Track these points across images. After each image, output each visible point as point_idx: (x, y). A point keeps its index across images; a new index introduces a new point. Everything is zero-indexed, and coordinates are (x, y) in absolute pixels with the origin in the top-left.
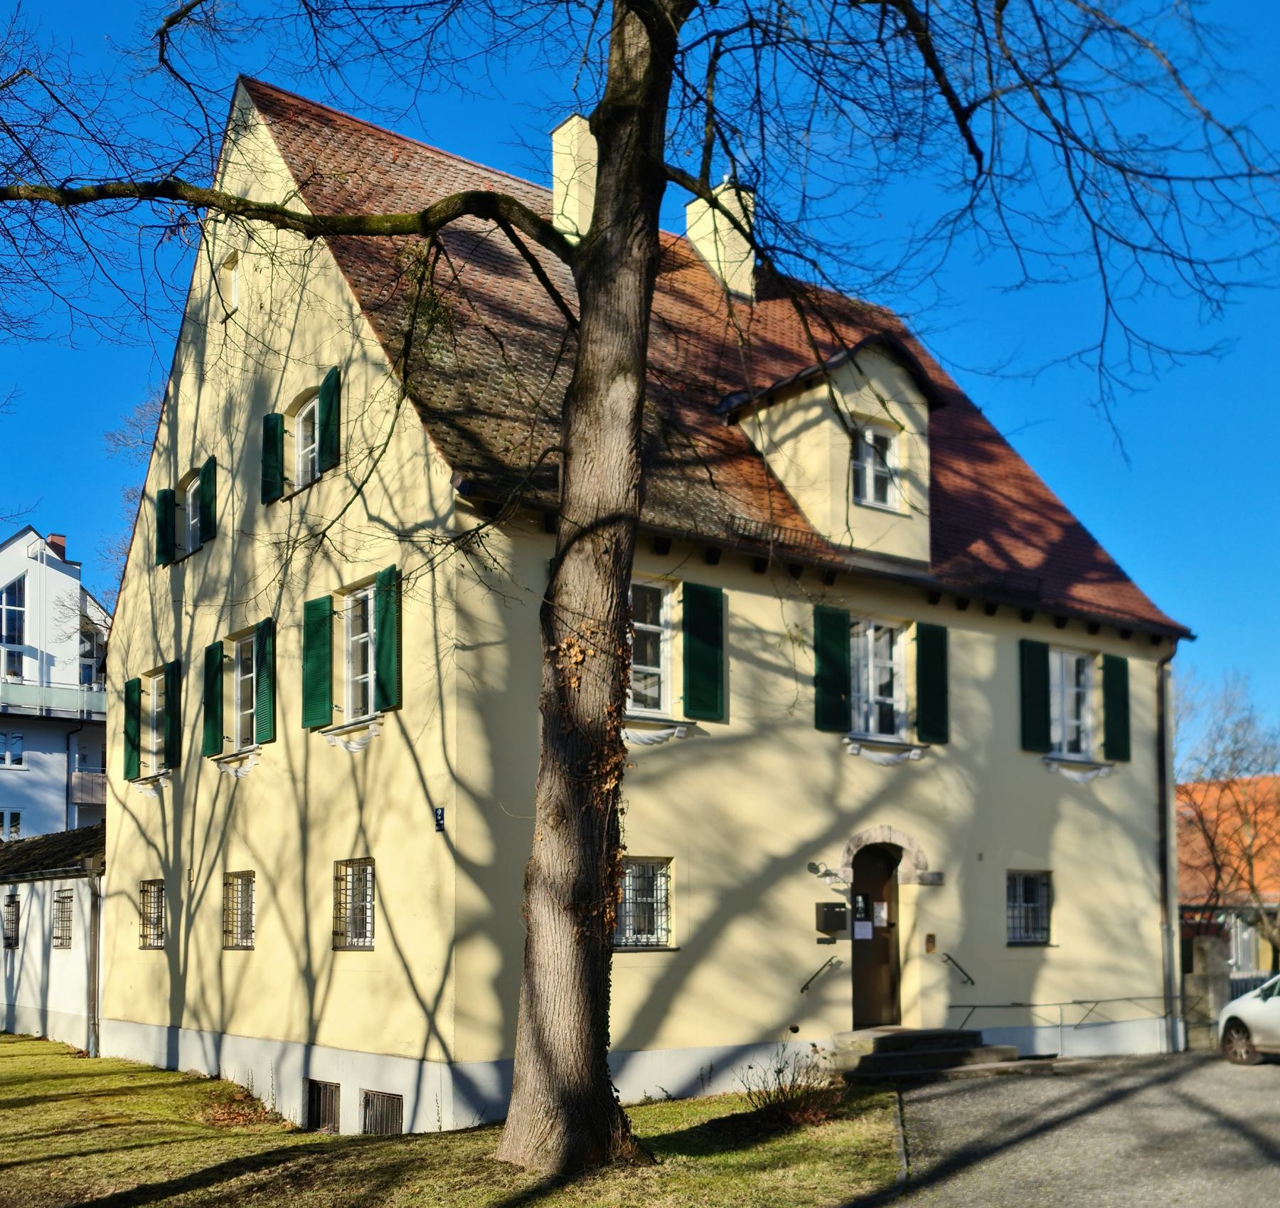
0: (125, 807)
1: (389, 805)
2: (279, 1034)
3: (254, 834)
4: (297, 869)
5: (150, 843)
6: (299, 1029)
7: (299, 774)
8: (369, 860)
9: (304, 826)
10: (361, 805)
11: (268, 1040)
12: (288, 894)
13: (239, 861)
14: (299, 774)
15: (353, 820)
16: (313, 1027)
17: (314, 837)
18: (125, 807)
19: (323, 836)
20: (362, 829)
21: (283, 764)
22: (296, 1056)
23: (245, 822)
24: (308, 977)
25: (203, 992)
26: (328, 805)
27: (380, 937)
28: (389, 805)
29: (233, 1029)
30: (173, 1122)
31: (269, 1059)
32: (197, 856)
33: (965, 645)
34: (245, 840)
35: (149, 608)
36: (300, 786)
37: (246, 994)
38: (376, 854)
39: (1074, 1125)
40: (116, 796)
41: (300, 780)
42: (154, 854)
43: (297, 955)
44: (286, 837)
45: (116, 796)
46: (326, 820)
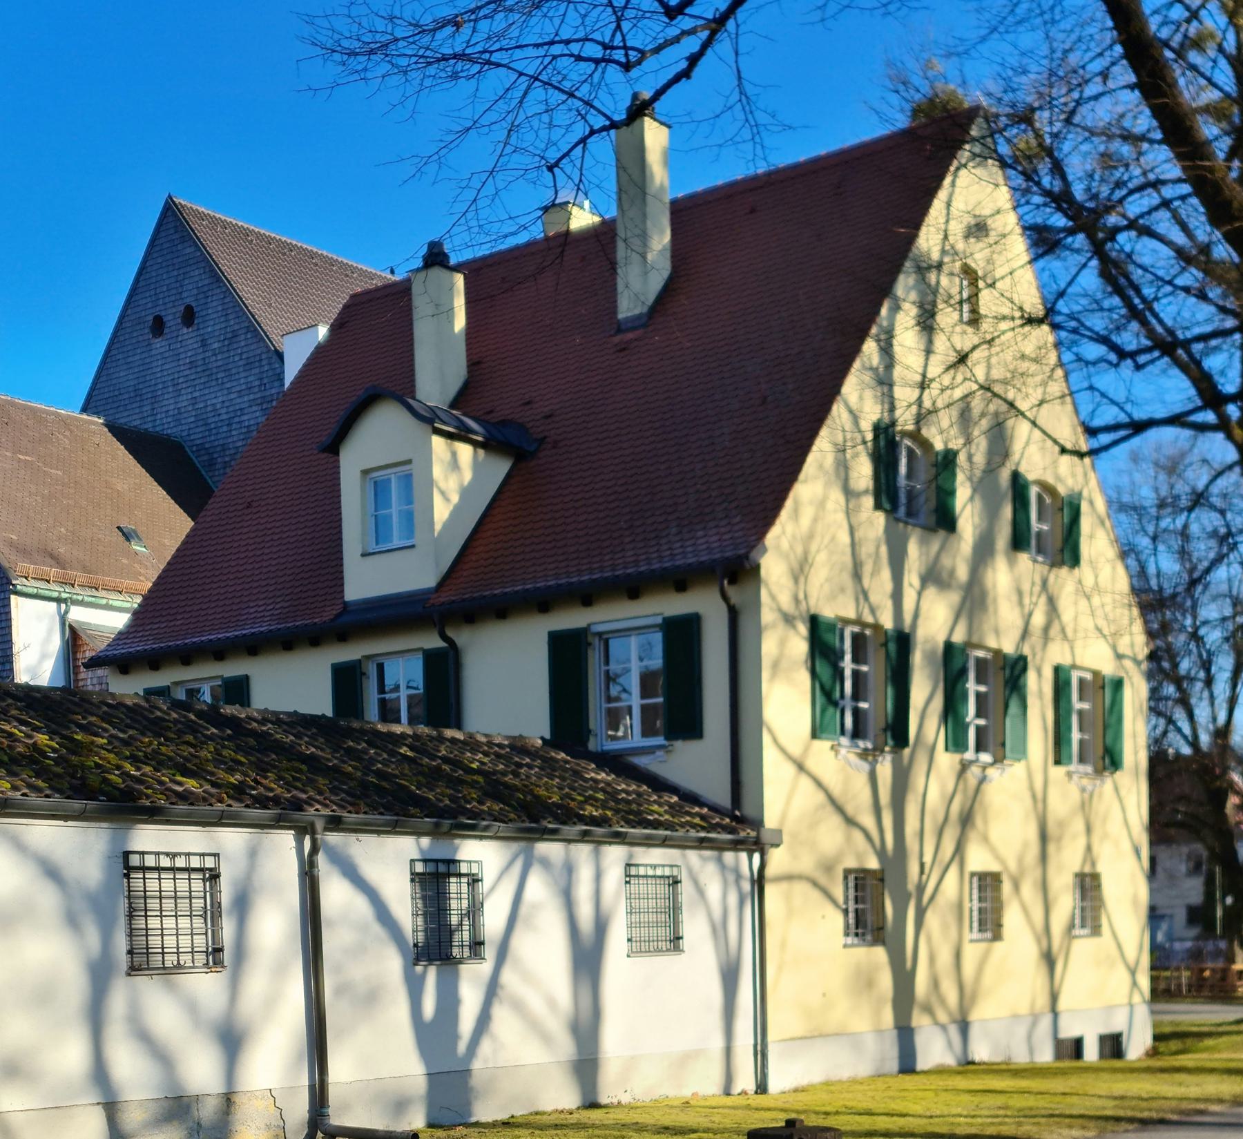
0: (801, 767)
1: (1105, 836)
2: (1024, 1009)
3: (995, 834)
4: (1037, 873)
5: (850, 821)
6: (1043, 1001)
7: (1039, 795)
8: (1095, 877)
9: (1044, 837)
10: (1089, 830)
11: (1015, 1017)
12: (1029, 890)
13: (978, 859)
14: (1039, 795)
15: (1081, 842)
16: (1054, 997)
17: (1051, 848)
18: (801, 767)
19: (1059, 849)
20: (1089, 848)
21: (1024, 784)
22: (1046, 1023)
23: (986, 822)
24: (1049, 960)
25: (935, 983)
26: (1061, 825)
27: (1105, 928)
28: (1105, 836)
29: (975, 1016)
30: (960, 1116)
31: (1021, 1031)
32: (924, 851)
33: (1033, 305)
34: (985, 839)
35: (845, 538)
36: (1040, 805)
37: (988, 979)
38: (1100, 868)
39: (1074, 888)
40: (783, 750)
41: (1040, 803)
42: (858, 836)
43: (1039, 941)
44: (1025, 845)
45: (783, 750)
46: (1059, 839)
